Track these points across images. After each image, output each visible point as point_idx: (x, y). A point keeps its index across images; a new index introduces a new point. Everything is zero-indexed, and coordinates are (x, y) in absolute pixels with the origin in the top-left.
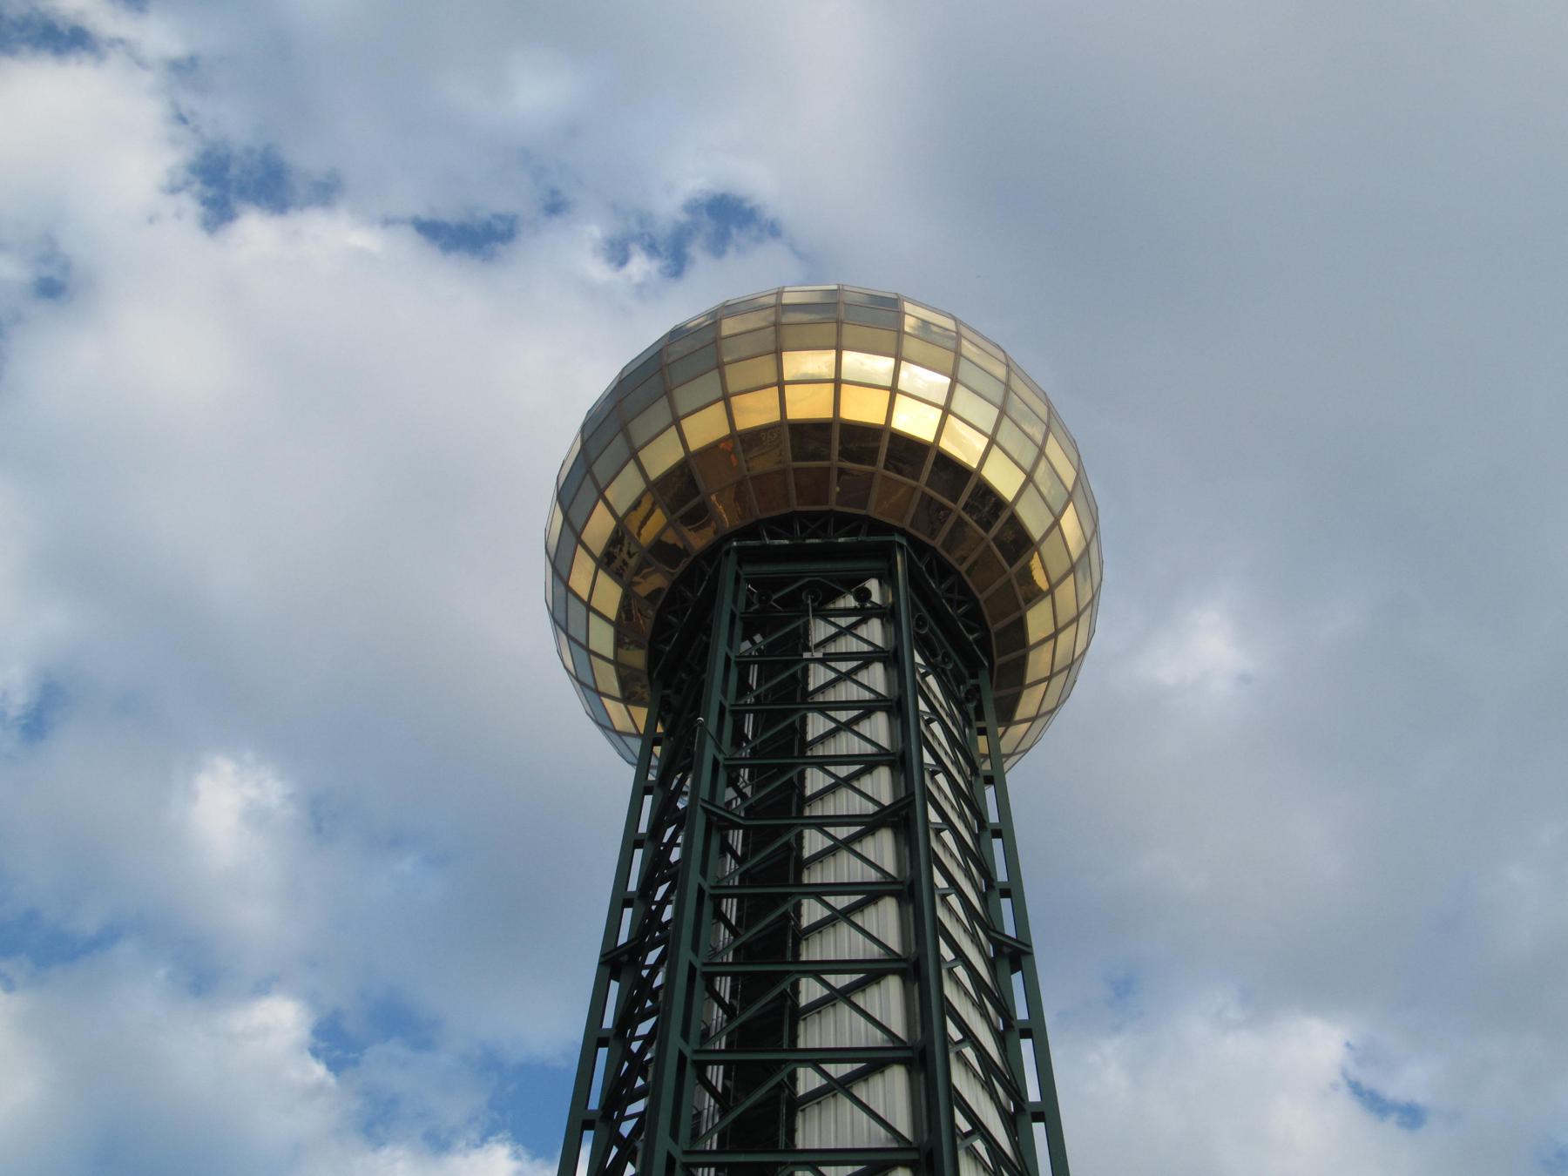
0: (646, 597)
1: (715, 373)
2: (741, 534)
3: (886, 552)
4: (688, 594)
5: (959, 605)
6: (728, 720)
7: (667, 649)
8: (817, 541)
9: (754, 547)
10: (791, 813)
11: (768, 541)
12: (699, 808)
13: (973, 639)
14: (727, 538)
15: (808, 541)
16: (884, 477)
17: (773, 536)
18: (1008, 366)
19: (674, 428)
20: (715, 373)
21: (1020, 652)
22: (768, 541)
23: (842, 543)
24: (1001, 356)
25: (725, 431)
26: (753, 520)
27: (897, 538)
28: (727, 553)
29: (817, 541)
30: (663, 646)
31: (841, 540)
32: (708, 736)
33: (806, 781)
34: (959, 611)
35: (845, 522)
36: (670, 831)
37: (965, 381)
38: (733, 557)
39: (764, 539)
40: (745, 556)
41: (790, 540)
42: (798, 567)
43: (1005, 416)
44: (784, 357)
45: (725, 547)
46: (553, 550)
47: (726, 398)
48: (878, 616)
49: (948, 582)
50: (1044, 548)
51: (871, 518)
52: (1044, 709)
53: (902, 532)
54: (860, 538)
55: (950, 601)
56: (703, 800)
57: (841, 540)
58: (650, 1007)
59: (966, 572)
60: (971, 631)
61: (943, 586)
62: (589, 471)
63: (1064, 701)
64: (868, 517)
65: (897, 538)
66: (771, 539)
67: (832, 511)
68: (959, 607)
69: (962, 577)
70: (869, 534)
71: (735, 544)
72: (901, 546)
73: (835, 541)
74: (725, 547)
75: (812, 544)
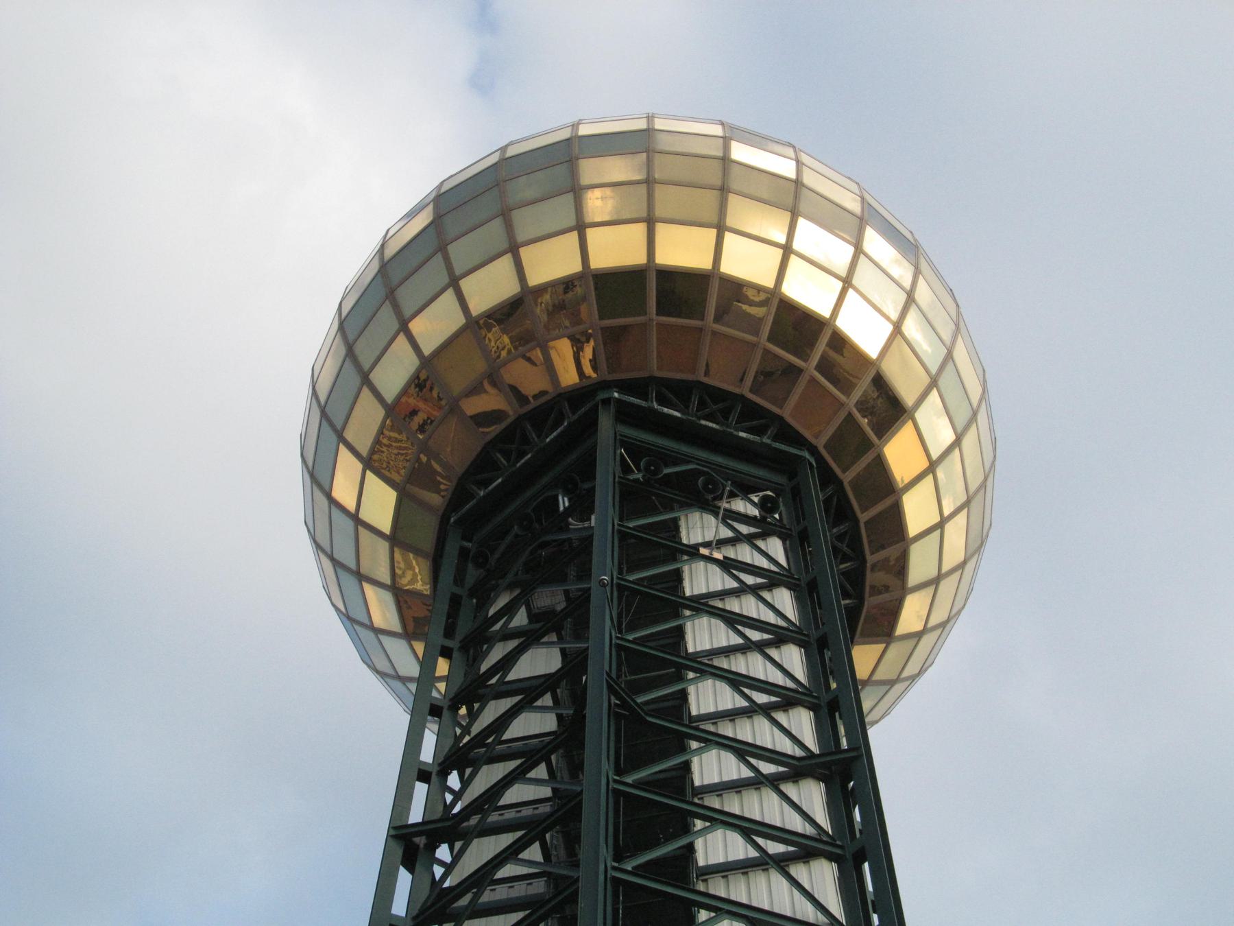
0: (471, 417)
1: (570, 196)
4: (534, 436)
7: (482, 493)
8: (714, 426)
9: (639, 407)
11: (656, 406)
15: (703, 422)
16: (813, 380)
17: (663, 401)
18: (957, 325)
19: (439, 255)
20: (570, 196)
21: (888, 502)
22: (656, 406)
23: (742, 438)
24: (854, 187)
25: (459, 321)
26: (647, 375)
27: (806, 454)
29: (714, 426)
30: (475, 488)
33: (689, 697)
34: (842, 566)
35: (754, 416)
36: (502, 601)
37: (942, 389)
39: (652, 402)
41: (683, 414)
42: (685, 449)
43: (914, 304)
44: (520, 251)
45: (602, 395)
46: (345, 312)
47: (513, 249)
50: (919, 415)
51: (784, 420)
52: (905, 674)
53: (813, 450)
54: (766, 440)
58: (476, 703)
59: (866, 523)
61: (835, 530)
62: (442, 249)
63: (926, 670)
64: (780, 419)
65: (806, 454)
66: (659, 405)
67: (743, 396)
70: (776, 438)
71: (616, 395)
73: (735, 433)
75: (706, 426)
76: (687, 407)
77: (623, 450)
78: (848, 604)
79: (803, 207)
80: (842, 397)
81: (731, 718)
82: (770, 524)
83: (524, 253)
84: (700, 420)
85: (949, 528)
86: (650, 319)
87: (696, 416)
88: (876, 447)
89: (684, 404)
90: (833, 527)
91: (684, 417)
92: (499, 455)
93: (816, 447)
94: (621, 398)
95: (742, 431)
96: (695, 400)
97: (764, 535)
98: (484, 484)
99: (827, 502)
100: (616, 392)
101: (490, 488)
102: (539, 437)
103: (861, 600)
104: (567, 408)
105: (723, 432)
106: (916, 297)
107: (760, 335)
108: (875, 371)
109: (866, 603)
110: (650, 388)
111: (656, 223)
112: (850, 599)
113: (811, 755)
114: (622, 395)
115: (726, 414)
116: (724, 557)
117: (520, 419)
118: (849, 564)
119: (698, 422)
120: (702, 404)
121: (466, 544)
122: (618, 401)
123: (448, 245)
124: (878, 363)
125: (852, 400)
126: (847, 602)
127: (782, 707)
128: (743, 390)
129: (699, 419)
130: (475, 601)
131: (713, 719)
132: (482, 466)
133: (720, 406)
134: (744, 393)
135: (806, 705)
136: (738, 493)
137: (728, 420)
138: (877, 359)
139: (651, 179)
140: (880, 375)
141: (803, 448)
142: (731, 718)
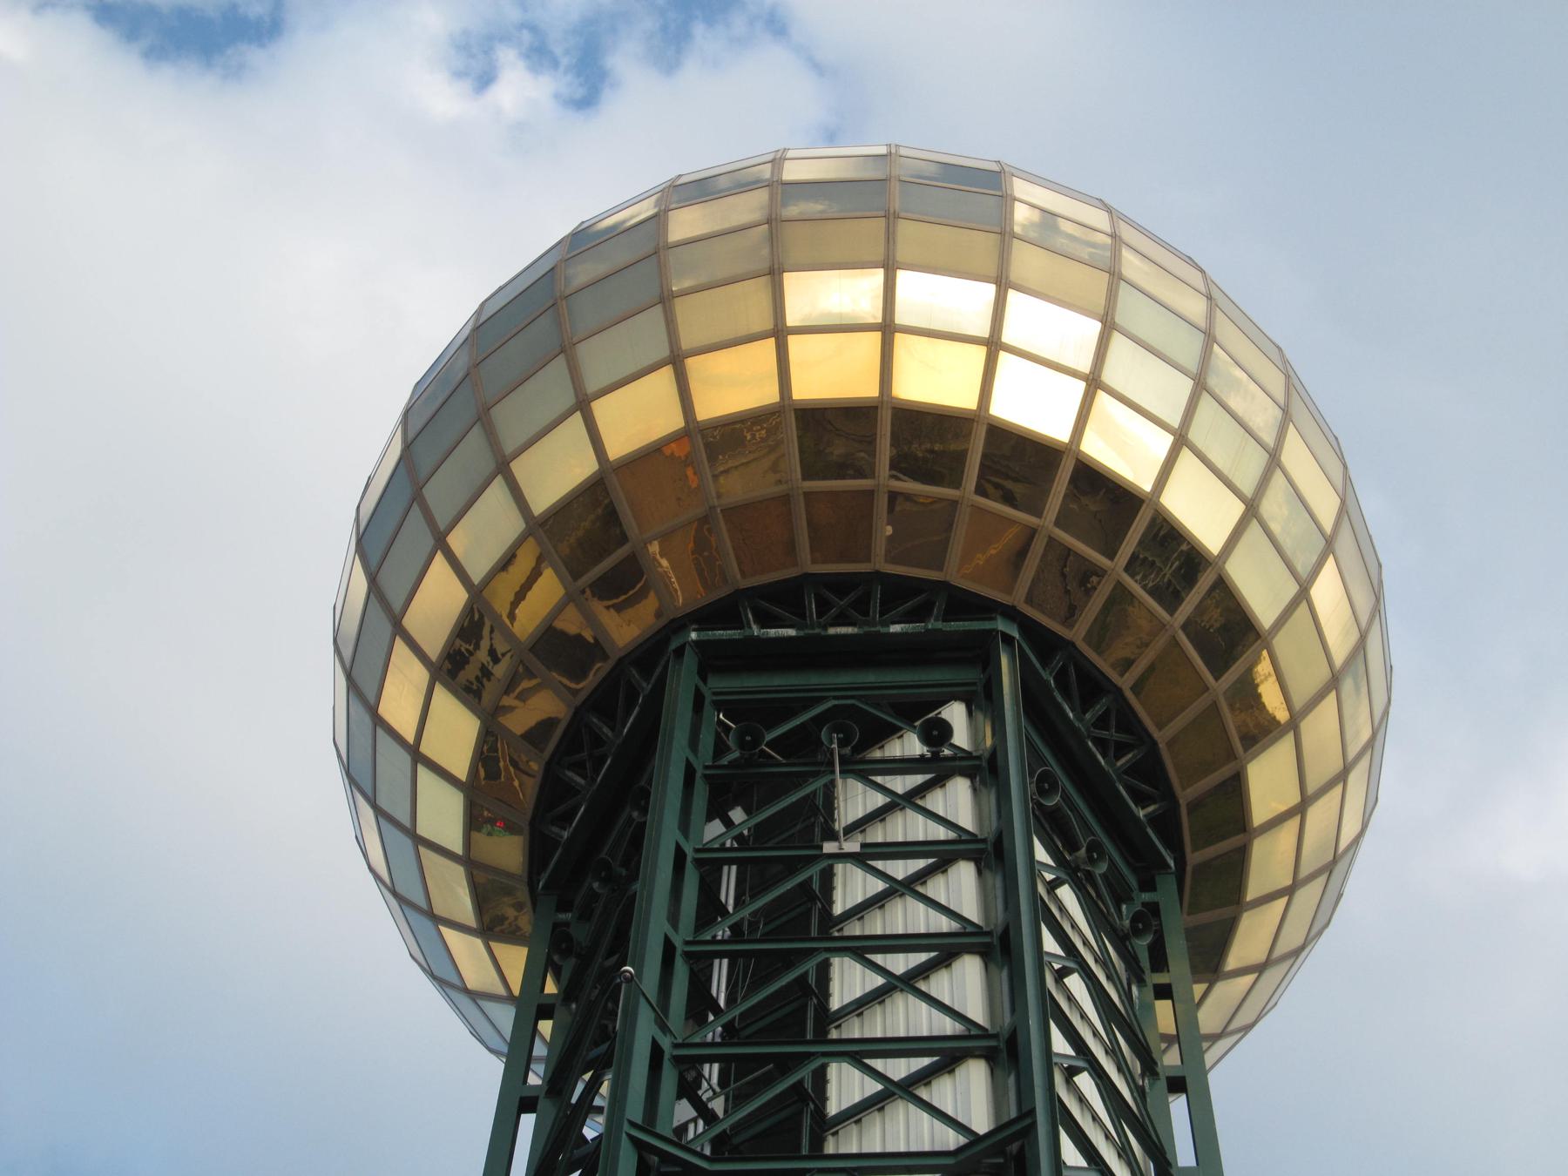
2: (705, 617)
3: (980, 652)
5: (1121, 749)
6: (681, 971)
7: (566, 835)
10: (798, 1147)
11: (756, 631)
12: (624, 1135)
13: (1145, 816)
14: (678, 626)
15: (832, 631)
17: (766, 620)
22: (756, 631)
23: (895, 634)
27: (1002, 625)
28: (679, 652)
31: (896, 628)
32: (642, 1001)
34: (1119, 764)
38: (690, 661)
39: (750, 627)
40: (713, 660)
42: (815, 679)
47: (676, 361)
48: (969, 773)
49: (1099, 709)
53: (1011, 613)
54: (932, 624)
55: (1101, 743)
56: (633, 1124)
57: (896, 628)
60: (1142, 800)
61: (1088, 716)
62: (418, 497)
64: (945, 586)
65: (1002, 625)
67: (877, 573)
68: (1117, 758)
69: (1125, 699)
71: (694, 635)
72: (1008, 640)
73: (883, 630)
74: (674, 645)
76: (803, 616)
77: (721, 716)
78: (1154, 811)
79: (902, 253)
80: (1031, 520)
81: (856, 1118)
82: (947, 759)
83: (692, 363)
84: (826, 630)
85: (1286, 458)
86: (710, 508)
87: (820, 626)
88: (1109, 572)
89: (798, 615)
90: (1084, 713)
91: (801, 633)
92: (570, 774)
93: (1014, 608)
94: (702, 638)
95: (894, 623)
96: (810, 603)
97: (939, 781)
98: (566, 819)
99: (1061, 677)
100: (694, 630)
101: (574, 825)
102: (612, 729)
103: (1170, 796)
104: (636, 676)
105: (867, 634)
106: (1117, 320)
107: (876, 475)
108: (1074, 461)
109: (1181, 801)
110: (741, 609)
111: (685, 360)
112: (1155, 803)
113: (975, 1139)
114: (703, 633)
115: (862, 606)
116: (863, 846)
117: (578, 715)
118: (1130, 756)
119: (823, 633)
120: (823, 606)
121: (562, 917)
122: (696, 643)
123: (421, 488)
124: (1074, 447)
125: (1048, 519)
126: (1151, 809)
127: (946, 1067)
128: (875, 564)
129: (825, 628)
130: (574, 1006)
131: (855, 1115)
132: (553, 795)
133: (852, 596)
134: (877, 567)
135: (977, 1053)
136: (899, 724)
137: (868, 615)
138: (1071, 441)
139: (666, 294)
140: (1083, 463)
141: (993, 615)
142: (856, 1118)
